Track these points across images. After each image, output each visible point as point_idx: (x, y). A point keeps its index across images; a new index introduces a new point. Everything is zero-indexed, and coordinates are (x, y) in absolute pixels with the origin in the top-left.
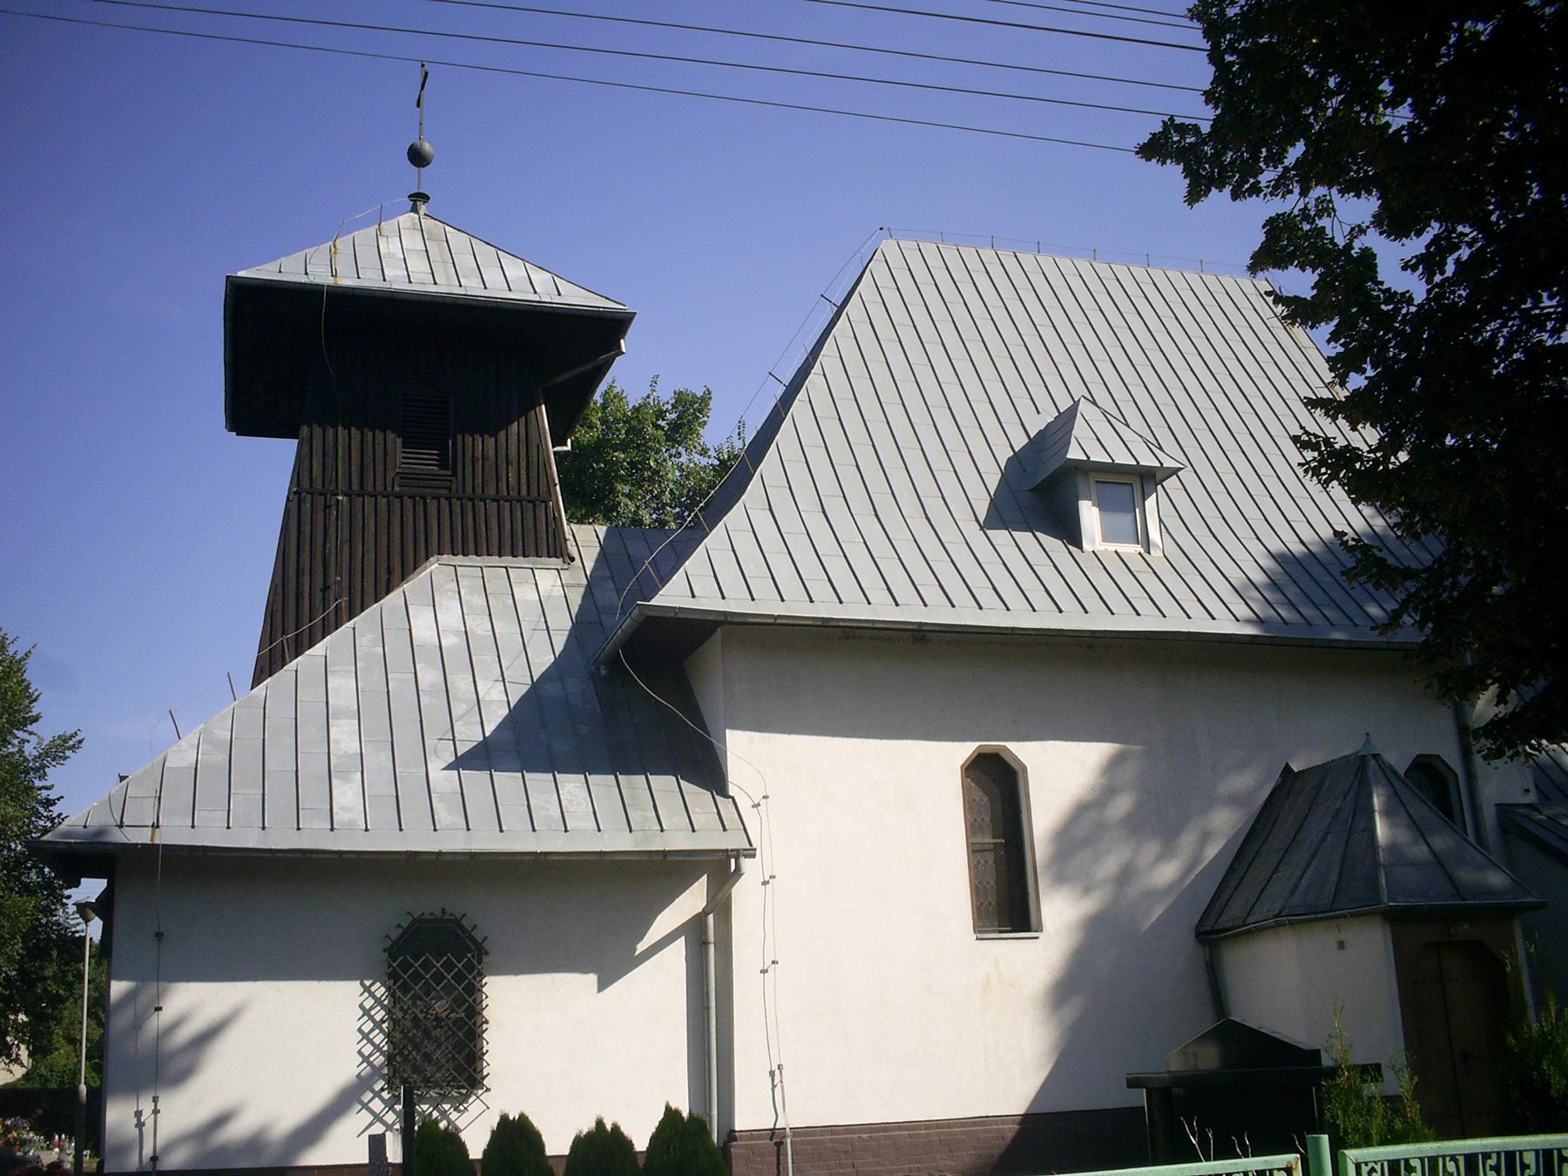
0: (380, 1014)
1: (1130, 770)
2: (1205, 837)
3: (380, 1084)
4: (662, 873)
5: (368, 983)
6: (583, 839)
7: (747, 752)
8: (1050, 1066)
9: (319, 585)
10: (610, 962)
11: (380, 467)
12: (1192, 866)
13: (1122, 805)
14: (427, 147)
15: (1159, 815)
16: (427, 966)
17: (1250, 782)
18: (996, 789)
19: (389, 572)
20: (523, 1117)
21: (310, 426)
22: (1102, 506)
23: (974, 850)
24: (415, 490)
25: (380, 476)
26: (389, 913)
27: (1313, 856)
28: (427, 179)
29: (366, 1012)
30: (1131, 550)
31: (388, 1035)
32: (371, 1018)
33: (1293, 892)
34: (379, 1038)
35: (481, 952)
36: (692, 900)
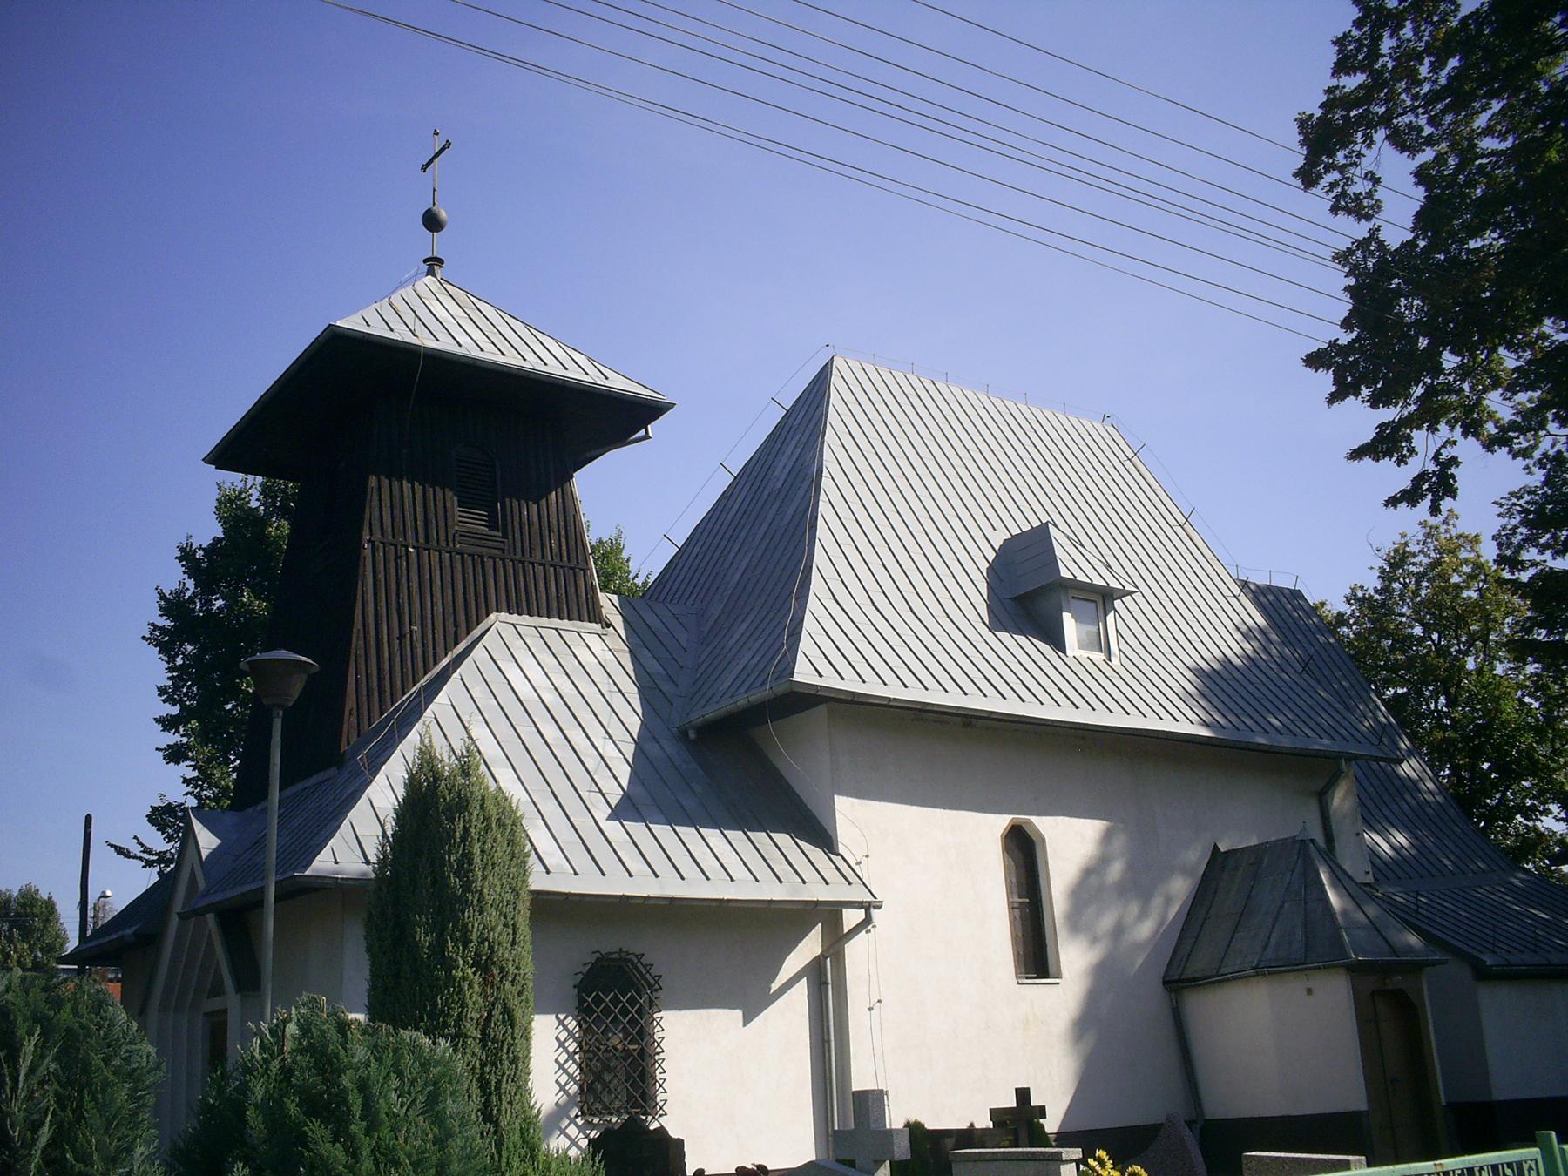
0: (572, 1047)
1: (1120, 842)
2: (1168, 900)
3: (575, 1111)
4: (786, 921)
5: (562, 1017)
6: (743, 890)
7: (853, 817)
8: (1072, 1092)
9: (396, 633)
10: (753, 1001)
11: (441, 524)
12: (1161, 924)
13: (1116, 870)
14: (443, 214)
15: (1139, 885)
16: (616, 1001)
17: (1196, 857)
18: (1023, 851)
19: (456, 626)
20: (680, 1143)
21: (378, 476)
22: (1076, 618)
23: (1012, 908)
24: (484, 550)
25: (442, 531)
26: (579, 951)
27: (1276, 918)
28: (439, 244)
29: (561, 1044)
30: (1099, 657)
31: (580, 1066)
32: (566, 1050)
33: (1265, 948)
34: (572, 1069)
35: (655, 986)
36: (810, 946)
